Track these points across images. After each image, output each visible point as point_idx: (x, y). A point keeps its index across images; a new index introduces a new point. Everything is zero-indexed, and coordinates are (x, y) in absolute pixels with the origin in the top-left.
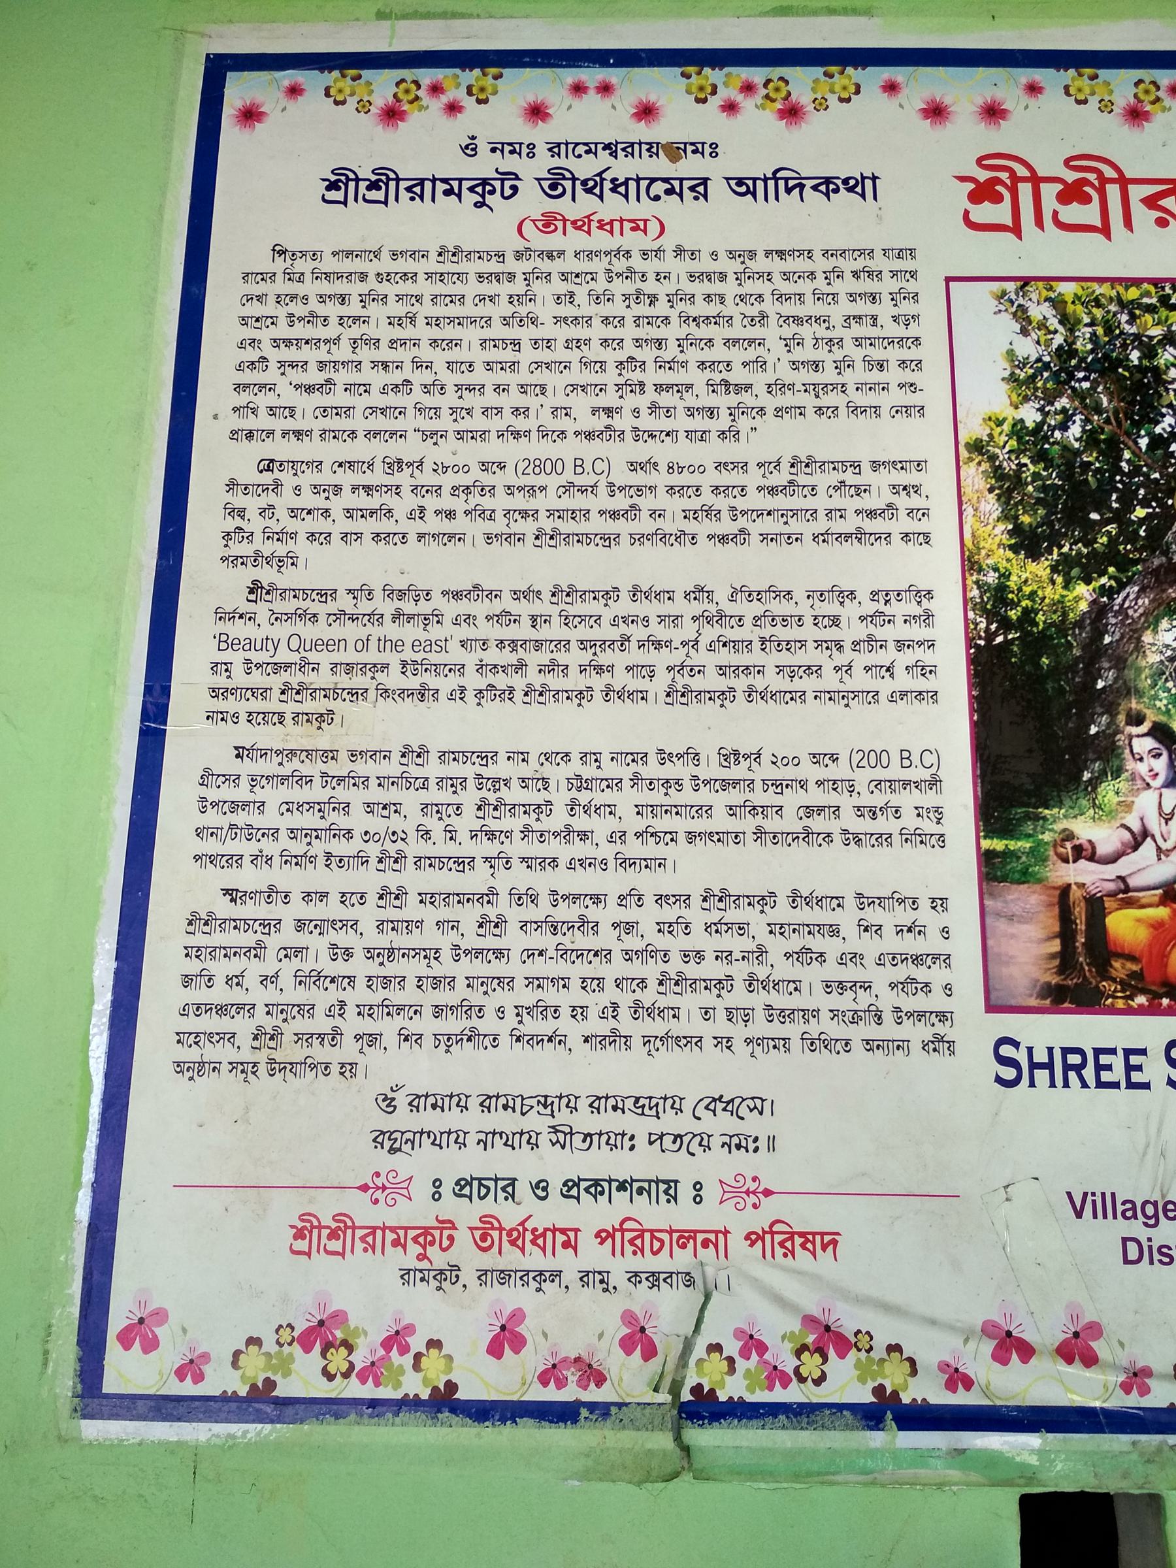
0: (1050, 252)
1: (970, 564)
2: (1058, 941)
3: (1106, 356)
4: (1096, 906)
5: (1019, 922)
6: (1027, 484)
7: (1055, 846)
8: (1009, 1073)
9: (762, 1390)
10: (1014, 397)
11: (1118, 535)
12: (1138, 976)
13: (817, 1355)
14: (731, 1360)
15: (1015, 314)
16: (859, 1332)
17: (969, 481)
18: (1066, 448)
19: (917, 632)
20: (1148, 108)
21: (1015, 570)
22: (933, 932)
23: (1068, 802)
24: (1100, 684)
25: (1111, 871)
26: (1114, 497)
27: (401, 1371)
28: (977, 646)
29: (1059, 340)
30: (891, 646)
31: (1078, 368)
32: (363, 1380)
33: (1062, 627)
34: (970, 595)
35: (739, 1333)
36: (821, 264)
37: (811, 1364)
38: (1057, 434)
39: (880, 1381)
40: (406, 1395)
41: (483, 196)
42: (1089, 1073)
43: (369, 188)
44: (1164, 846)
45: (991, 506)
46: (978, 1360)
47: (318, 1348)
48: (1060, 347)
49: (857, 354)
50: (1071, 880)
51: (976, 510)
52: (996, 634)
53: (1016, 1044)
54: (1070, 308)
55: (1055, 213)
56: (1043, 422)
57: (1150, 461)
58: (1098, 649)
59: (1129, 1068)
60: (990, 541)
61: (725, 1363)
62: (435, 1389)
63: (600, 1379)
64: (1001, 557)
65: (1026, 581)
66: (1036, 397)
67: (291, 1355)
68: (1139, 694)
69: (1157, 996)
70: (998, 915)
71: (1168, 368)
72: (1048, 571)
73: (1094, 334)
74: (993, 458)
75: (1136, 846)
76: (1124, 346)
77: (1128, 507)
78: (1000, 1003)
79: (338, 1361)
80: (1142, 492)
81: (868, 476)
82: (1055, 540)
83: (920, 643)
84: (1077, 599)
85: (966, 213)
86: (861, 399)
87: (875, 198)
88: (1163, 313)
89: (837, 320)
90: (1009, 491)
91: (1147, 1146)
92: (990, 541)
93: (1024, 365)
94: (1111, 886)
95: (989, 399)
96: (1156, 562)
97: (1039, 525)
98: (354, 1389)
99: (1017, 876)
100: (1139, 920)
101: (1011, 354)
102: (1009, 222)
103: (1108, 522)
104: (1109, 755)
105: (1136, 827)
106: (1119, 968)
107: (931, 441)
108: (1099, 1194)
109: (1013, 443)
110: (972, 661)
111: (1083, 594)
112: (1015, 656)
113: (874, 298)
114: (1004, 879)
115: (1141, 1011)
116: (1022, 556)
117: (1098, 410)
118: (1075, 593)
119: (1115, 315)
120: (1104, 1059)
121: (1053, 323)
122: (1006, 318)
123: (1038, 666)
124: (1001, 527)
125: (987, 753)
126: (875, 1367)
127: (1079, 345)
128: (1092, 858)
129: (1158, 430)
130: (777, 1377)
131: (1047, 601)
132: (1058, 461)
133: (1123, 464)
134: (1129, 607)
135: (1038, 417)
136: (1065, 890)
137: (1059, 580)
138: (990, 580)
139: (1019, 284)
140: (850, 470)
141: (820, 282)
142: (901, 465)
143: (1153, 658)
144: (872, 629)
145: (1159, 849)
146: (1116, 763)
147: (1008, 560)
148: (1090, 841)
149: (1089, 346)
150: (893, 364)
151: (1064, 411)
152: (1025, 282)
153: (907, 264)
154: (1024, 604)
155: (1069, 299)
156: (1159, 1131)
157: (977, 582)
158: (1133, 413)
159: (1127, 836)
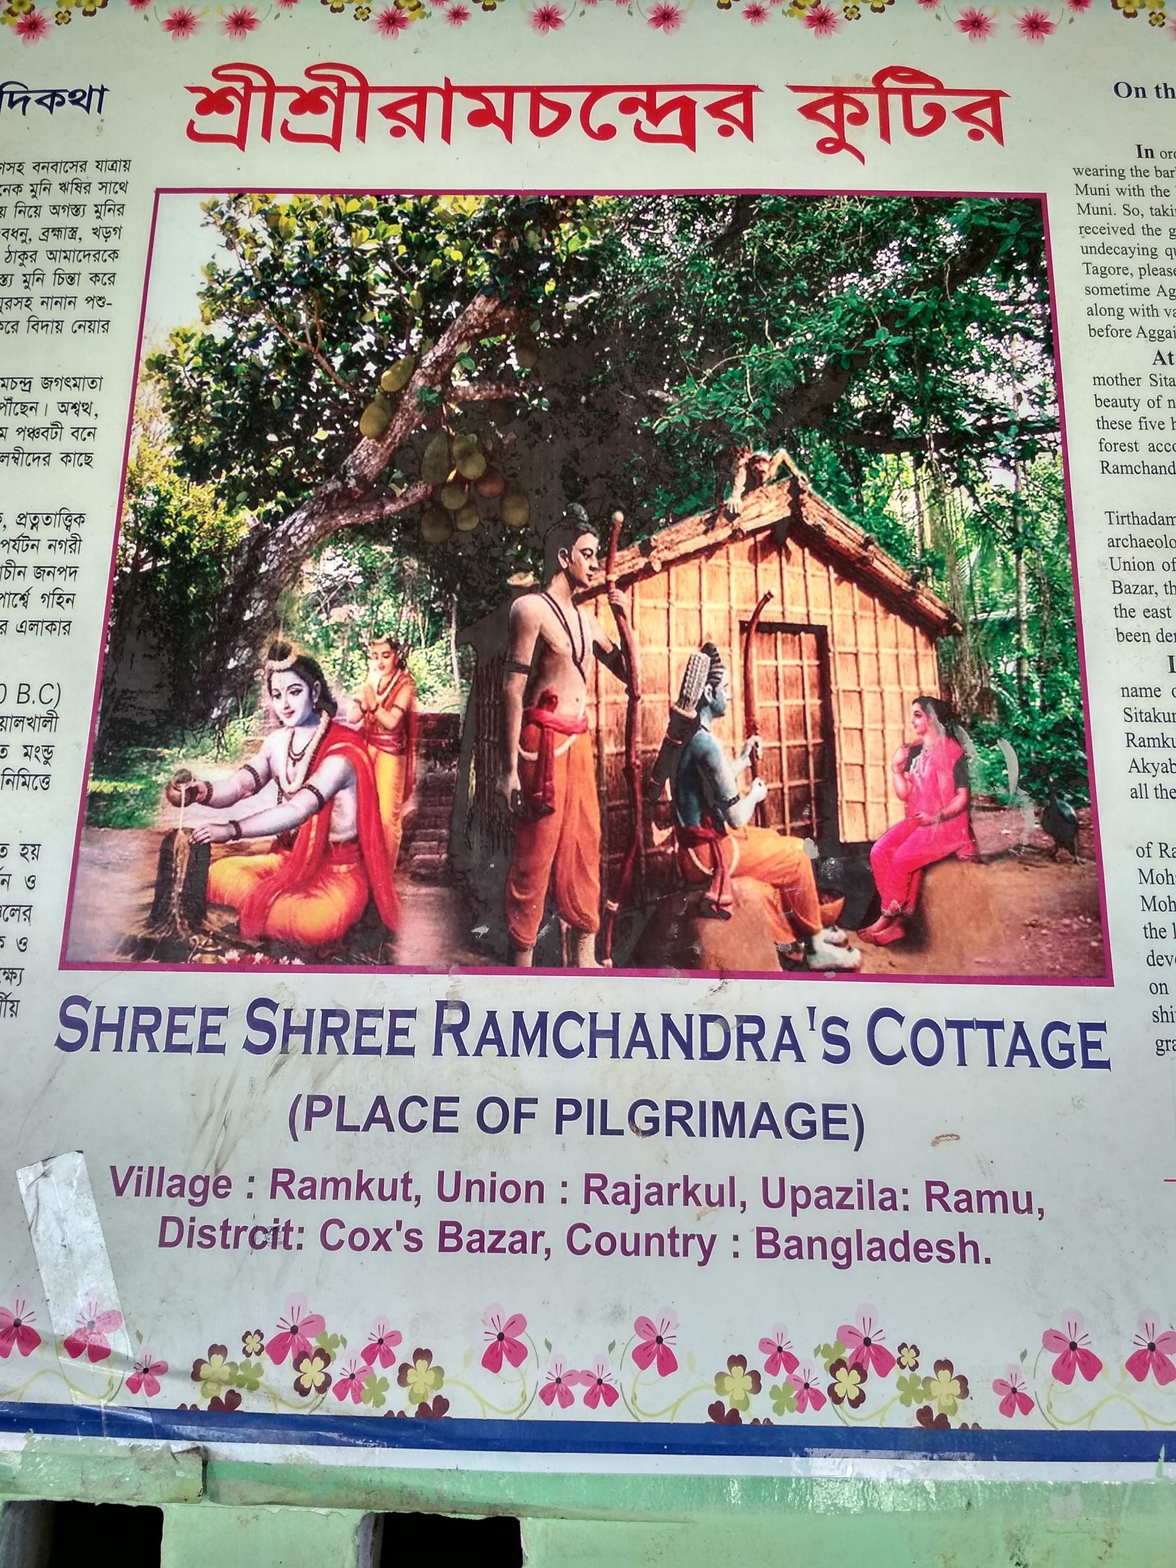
0: (286, 166)
1: (130, 485)
2: (152, 891)
3: (313, 271)
4: (201, 853)
5: (114, 870)
6: (205, 403)
7: (168, 789)
8: (72, 1036)
9: (791, 1411)
10: (208, 312)
11: (294, 458)
12: (235, 929)
13: (854, 1372)
14: (755, 1375)
15: (223, 227)
16: (904, 1345)
17: (145, 399)
18: (254, 366)
19: (60, 558)
20: (407, 14)
21: (177, 494)
22: (18, 882)
23: (190, 741)
24: (248, 615)
25: (223, 816)
26: (296, 418)
27: (384, 1384)
28: (123, 575)
29: (265, 253)
30: (30, 572)
31: (280, 283)
32: (341, 1394)
33: (216, 556)
34: (124, 519)
35: (765, 1344)
36: (31, 176)
37: (847, 1382)
38: (247, 352)
39: (925, 1403)
40: (390, 1412)
41: (838, 126)
42: (160, 1036)
43: (296, 108)
44: (287, 788)
45: (163, 426)
46: (1037, 1378)
47: (290, 1357)
48: (266, 261)
49: (48, 267)
50: (179, 825)
51: (145, 430)
52: (145, 561)
53: (273, 1006)
54: (283, 220)
55: (286, 123)
56: (234, 339)
57: (341, 381)
58: (252, 578)
59: (394, 1032)
60: (155, 462)
61: (749, 1378)
62: (423, 1406)
63: (611, 1396)
64: (165, 480)
65: (186, 506)
66: (231, 312)
67: (259, 1366)
68: (288, 626)
69: (252, 951)
70: (93, 862)
71: (376, 283)
72: (213, 494)
73: (305, 248)
74: (173, 375)
75: (255, 791)
76: (334, 260)
77: (309, 425)
78: (77, 959)
79: (313, 1371)
80: (327, 413)
81: (38, 394)
82: (225, 462)
83: (62, 570)
84: (238, 526)
85: (192, 123)
86: (44, 314)
87: (99, 111)
88: (382, 225)
89: (35, 232)
90: (186, 410)
91: (210, 1115)
92: (155, 462)
93: (224, 279)
94: (222, 832)
95: (181, 312)
96: (330, 487)
97: (211, 447)
98: (332, 1405)
99: (120, 820)
100: (245, 868)
101: (212, 267)
102: (234, 133)
103: (285, 444)
104: (244, 689)
105: (260, 768)
106: (215, 920)
107: (111, 358)
108: (146, 1169)
109: (199, 360)
110: (114, 589)
111: (247, 518)
112: (161, 585)
113: (77, 210)
114: (106, 824)
115: (232, 967)
116: (187, 479)
117: (294, 327)
118: (237, 519)
119: (329, 228)
120: (180, 1020)
121: (263, 236)
122: (214, 229)
123: (184, 595)
124: (170, 448)
125: (112, 688)
126: (920, 1387)
127: (285, 260)
128: (206, 802)
129: (355, 348)
130: (810, 1396)
131: (206, 526)
132: (243, 380)
133: (312, 384)
134: (294, 534)
135: (230, 334)
136: (171, 836)
137: (223, 504)
138: (148, 504)
139: (233, 195)
140: (19, 386)
141: (26, 197)
142: (73, 382)
143: (310, 588)
144: (13, 554)
145: (281, 791)
146: (250, 699)
147: (172, 483)
148: (208, 784)
149: (297, 261)
150: (85, 278)
151: (258, 327)
152: (240, 193)
153: (119, 176)
154: (180, 530)
155: (283, 212)
156: (226, 1099)
157: (134, 507)
158: (332, 330)
159: (249, 777)
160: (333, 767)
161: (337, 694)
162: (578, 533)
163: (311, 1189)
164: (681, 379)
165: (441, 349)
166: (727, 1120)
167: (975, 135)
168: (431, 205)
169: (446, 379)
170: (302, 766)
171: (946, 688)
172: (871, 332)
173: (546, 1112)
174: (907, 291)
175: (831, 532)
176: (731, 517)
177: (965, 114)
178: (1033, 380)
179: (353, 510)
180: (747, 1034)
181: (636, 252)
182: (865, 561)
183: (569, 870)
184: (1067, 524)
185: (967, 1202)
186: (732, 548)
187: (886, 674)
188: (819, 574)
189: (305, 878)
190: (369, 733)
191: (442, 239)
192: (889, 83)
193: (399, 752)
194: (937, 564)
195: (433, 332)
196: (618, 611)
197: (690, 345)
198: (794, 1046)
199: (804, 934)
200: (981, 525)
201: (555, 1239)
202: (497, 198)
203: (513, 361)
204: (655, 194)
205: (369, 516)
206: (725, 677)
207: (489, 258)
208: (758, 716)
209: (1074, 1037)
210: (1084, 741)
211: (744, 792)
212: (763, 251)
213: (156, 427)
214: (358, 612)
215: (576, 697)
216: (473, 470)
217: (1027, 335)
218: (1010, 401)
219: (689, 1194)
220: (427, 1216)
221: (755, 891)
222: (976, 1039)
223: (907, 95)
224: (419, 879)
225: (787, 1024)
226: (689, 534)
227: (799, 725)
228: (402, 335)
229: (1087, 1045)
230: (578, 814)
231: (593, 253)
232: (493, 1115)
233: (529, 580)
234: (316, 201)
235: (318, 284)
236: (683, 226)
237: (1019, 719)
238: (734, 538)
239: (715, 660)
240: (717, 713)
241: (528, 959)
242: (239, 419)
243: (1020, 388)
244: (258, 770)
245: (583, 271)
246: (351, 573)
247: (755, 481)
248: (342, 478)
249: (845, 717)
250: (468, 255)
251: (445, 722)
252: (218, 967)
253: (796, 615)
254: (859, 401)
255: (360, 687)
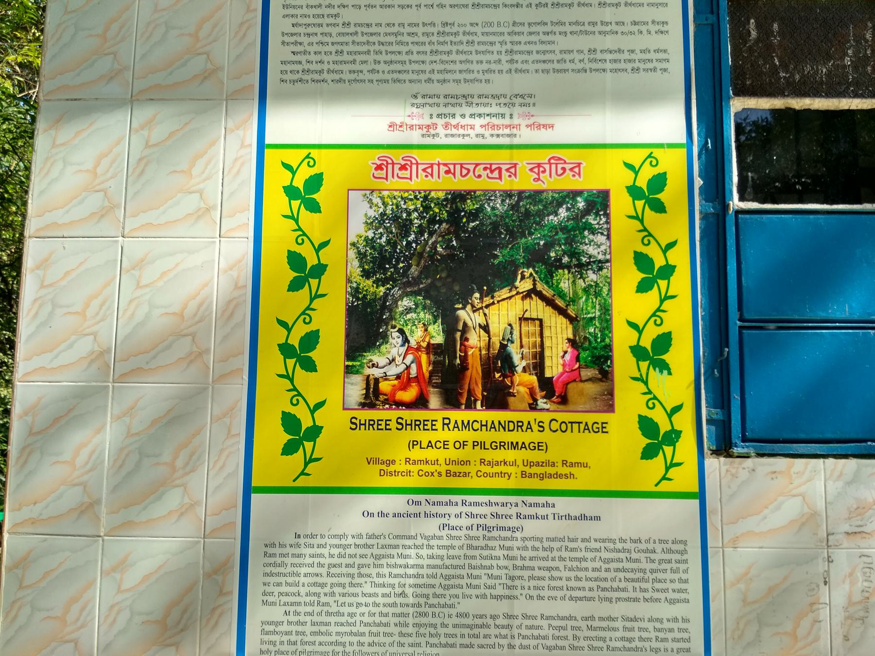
1: (349, 281)
4: (377, 381)
18: (380, 244)
25: (382, 371)
29: (381, 210)
33: (374, 300)
45: (356, 263)
59: (386, 425)
68: (395, 319)
74: (358, 248)
77: (398, 262)
82: (375, 273)
104: (385, 337)
106: (382, 398)
110: (347, 310)
111: (382, 290)
115: (387, 409)
117: (391, 233)
121: (380, 204)
143: (401, 309)
152: (373, 191)
160: (410, 358)
161: (410, 338)
162: (474, 293)
163: (415, 462)
164: (502, 248)
165: (434, 239)
166: (514, 446)
167: (574, 176)
168: (429, 194)
169: (435, 248)
170: (402, 357)
171: (575, 336)
172: (557, 234)
173: (470, 444)
174: (568, 221)
175: (544, 292)
176: (516, 288)
177: (571, 169)
178: (603, 248)
179: (410, 287)
180: (519, 425)
181: (489, 209)
182: (554, 300)
183: (473, 386)
184: (610, 290)
185: (572, 465)
186: (517, 297)
187: (558, 332)
188: (541, 304)
189: (404, 387)
190: (418, 349)
191: (432, 205)
192: (552, 161)
193: (427, 354)
194: (573, 301)
195: (431, 234)
196: (485, 315)
197: (505, 238)
198: (531, 428)
199: (535, 400)
200: (586, 290)
201: (473, 474)
202: (448, 192)
203: (454, 243)
204: (495, 191)
205: (416, 289)
206: (515, 333)
207: (447, 211)
208: (524, 343)
209: (600, 426)
210: (611, 350)
211: (520, 363)
212: (526, 209)
213: (354, 263)
214: (414, 315)
215: (475, 339)
216: (444, 275)
217: (602, 234)
218: (596, 254)
219: (505, 463)
220: (443, 469)
221: (523, 390)
222: (575, 426)
223: (557, 164)
224: (434, 387)
225: (529, 423)
226: (504, 293)
227: (535, 346)
228: (423, 235)
229: (603, 428)
230: (475, 370)
231: (477, 209)
232: (457, 445)
233: (460, 306)
234: (396, 193)
235: (397, 220)
236: (503, 201)
237: (594, 344)
238: (518, 293)
239: (512, 328)
240: (512, 342)
241: (463, 407)
242: (378, 261)
243: (599, 250)
244: (390, 359)
245: (473, 215)
246: (412, 305)
247: (523, 278)
248: (408, 277)
249: (547, 343)
250: (440, 210)
251: (439, 345)
252: (384, 409)
253: (534, 316)
254: (553, 254)
255: (416, 336)
